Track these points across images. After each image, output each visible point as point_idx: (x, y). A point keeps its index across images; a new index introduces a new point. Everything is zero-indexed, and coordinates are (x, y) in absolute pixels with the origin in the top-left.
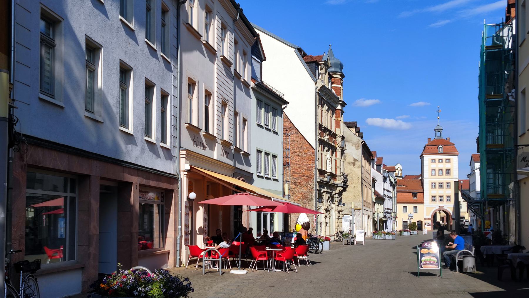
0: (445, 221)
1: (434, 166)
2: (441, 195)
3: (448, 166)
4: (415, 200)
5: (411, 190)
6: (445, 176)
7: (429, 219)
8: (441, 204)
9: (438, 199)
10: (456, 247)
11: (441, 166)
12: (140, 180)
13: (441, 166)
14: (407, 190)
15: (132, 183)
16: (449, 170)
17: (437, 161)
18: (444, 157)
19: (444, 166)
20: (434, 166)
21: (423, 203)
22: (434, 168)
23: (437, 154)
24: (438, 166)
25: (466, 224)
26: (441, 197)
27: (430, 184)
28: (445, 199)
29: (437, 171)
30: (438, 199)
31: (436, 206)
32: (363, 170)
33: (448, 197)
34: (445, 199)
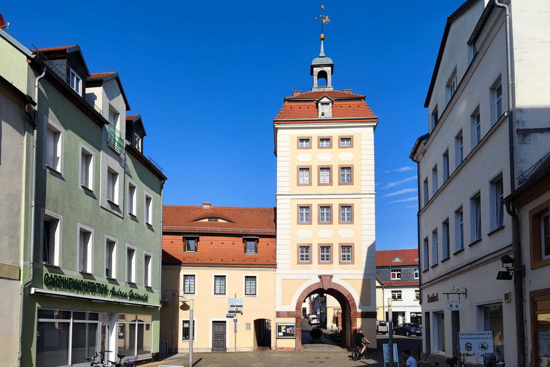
0: (340, 323)
1: (306, 157)
2: (325, 242)
3: (345, 157)
4: (250, 258)
5: (241, 231)
6: (336, 188)
7: (289, 314)
8: (325, 270)
9: (315, 253)
10: (30, 290)
11: (325, 157)
12: (329, 71)
13: (325, 157)
14: (230, 230)
15: (59, 220)
16: (349, 168)
17: (335, 142)
18: (336, 133)
19: (336, 157)
20: (306, 157)
21: (274, 266)
22: (325, 164)
23: (315, 120)
24: (316, 157)
25: (381, 329)
26: (325, 248)
27: (295, 211)
28: (336, 253)
29: (315, 171)
30: (315, 253)
31: (311, 275)
32: (484, 132)
33: (347, 248)
34: (336, 253)
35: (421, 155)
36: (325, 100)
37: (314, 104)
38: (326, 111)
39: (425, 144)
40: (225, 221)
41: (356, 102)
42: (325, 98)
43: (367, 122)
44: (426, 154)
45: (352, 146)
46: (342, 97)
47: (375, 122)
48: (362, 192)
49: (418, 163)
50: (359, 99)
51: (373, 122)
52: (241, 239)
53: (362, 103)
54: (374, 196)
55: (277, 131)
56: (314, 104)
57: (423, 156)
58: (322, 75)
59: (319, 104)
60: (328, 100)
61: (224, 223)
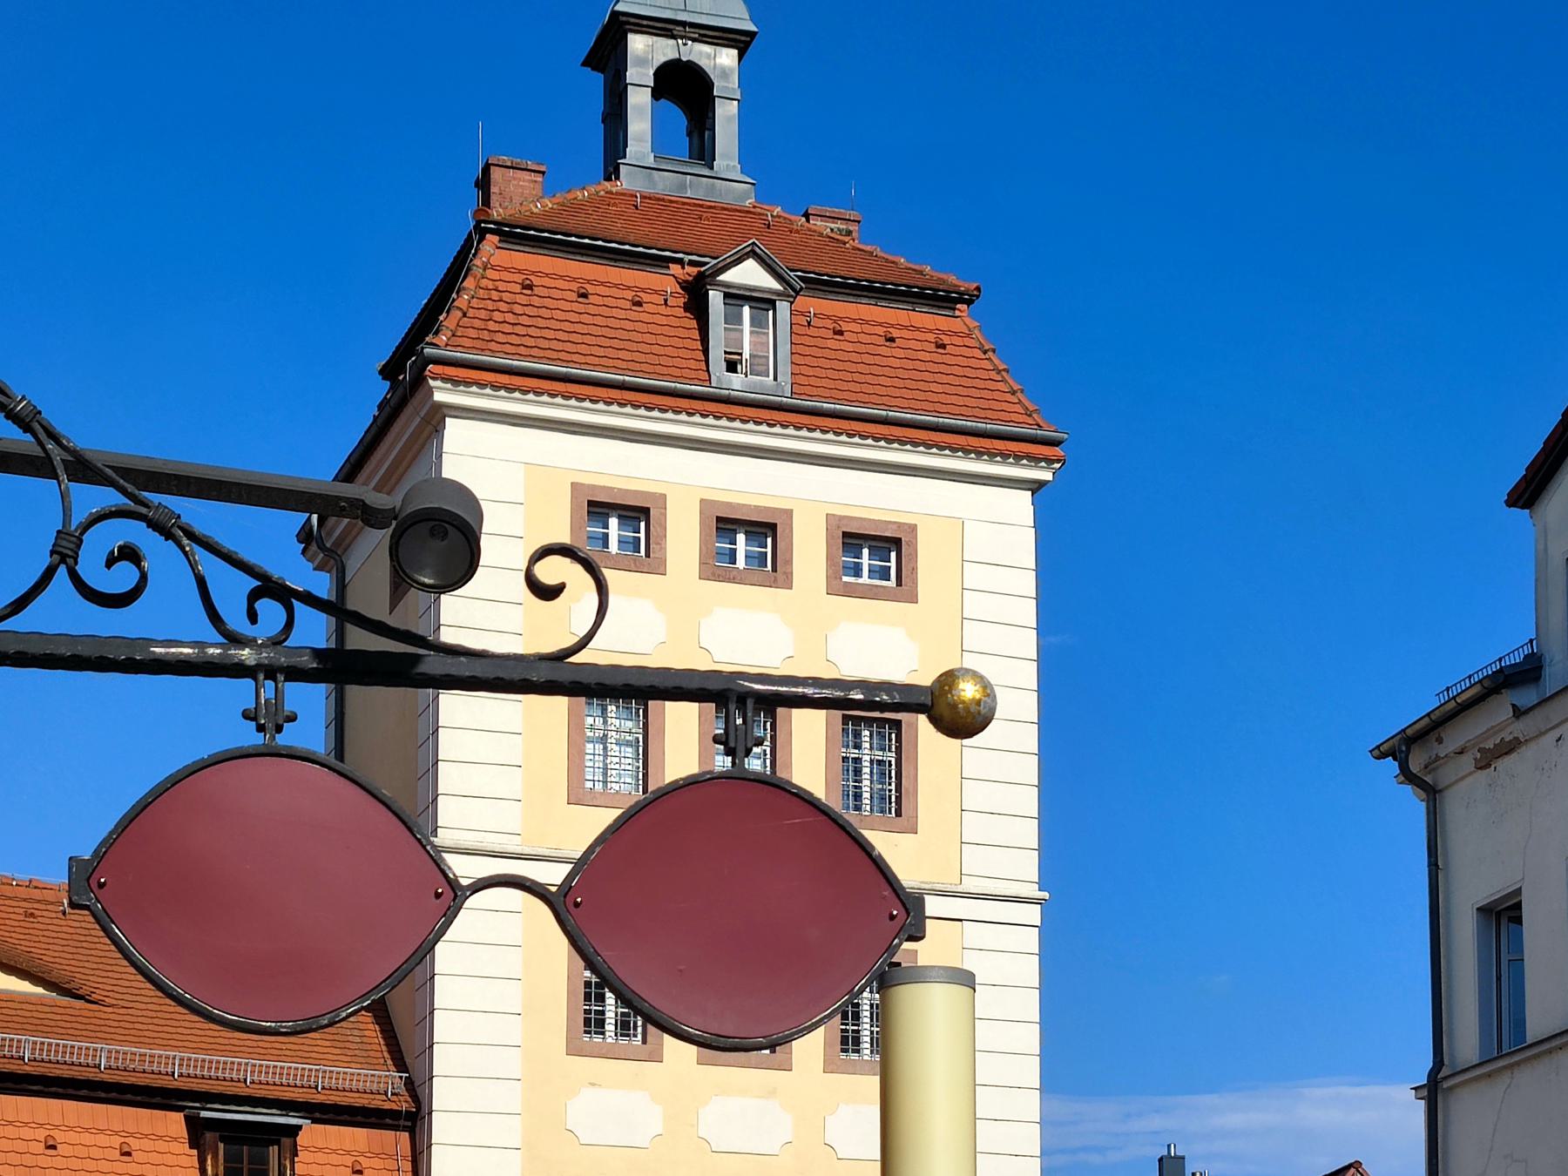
12: (725, 73)
18: (816, 492)
23: (681, 393)
35: (1467, 761)
36: (749, 274)
37: (666, 282)
38: (756, 350)
39: (1518, 713)
40: (40, 990)
41: (925, 318)
42: (750, 264)
43: (1005, 456)
44: (1504, 764)
45: (904, 587)
46: (827, 267)
47: (1049, 461)
48: (970, 885)
49: (1432, 793)
50: (944, 299)
51: (1035, 460)
52: (174, 1123)
53: (956, 325)
54: (1033, 914)
55: (439, 429)
56: (666, 282)
57: (1483, 765)
58: (684, 87)
59: (715, 298)
60: (769, 282)
61: (25, 999)
